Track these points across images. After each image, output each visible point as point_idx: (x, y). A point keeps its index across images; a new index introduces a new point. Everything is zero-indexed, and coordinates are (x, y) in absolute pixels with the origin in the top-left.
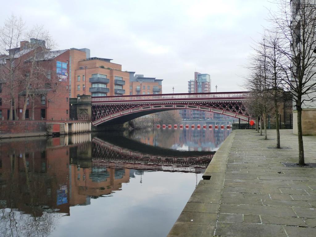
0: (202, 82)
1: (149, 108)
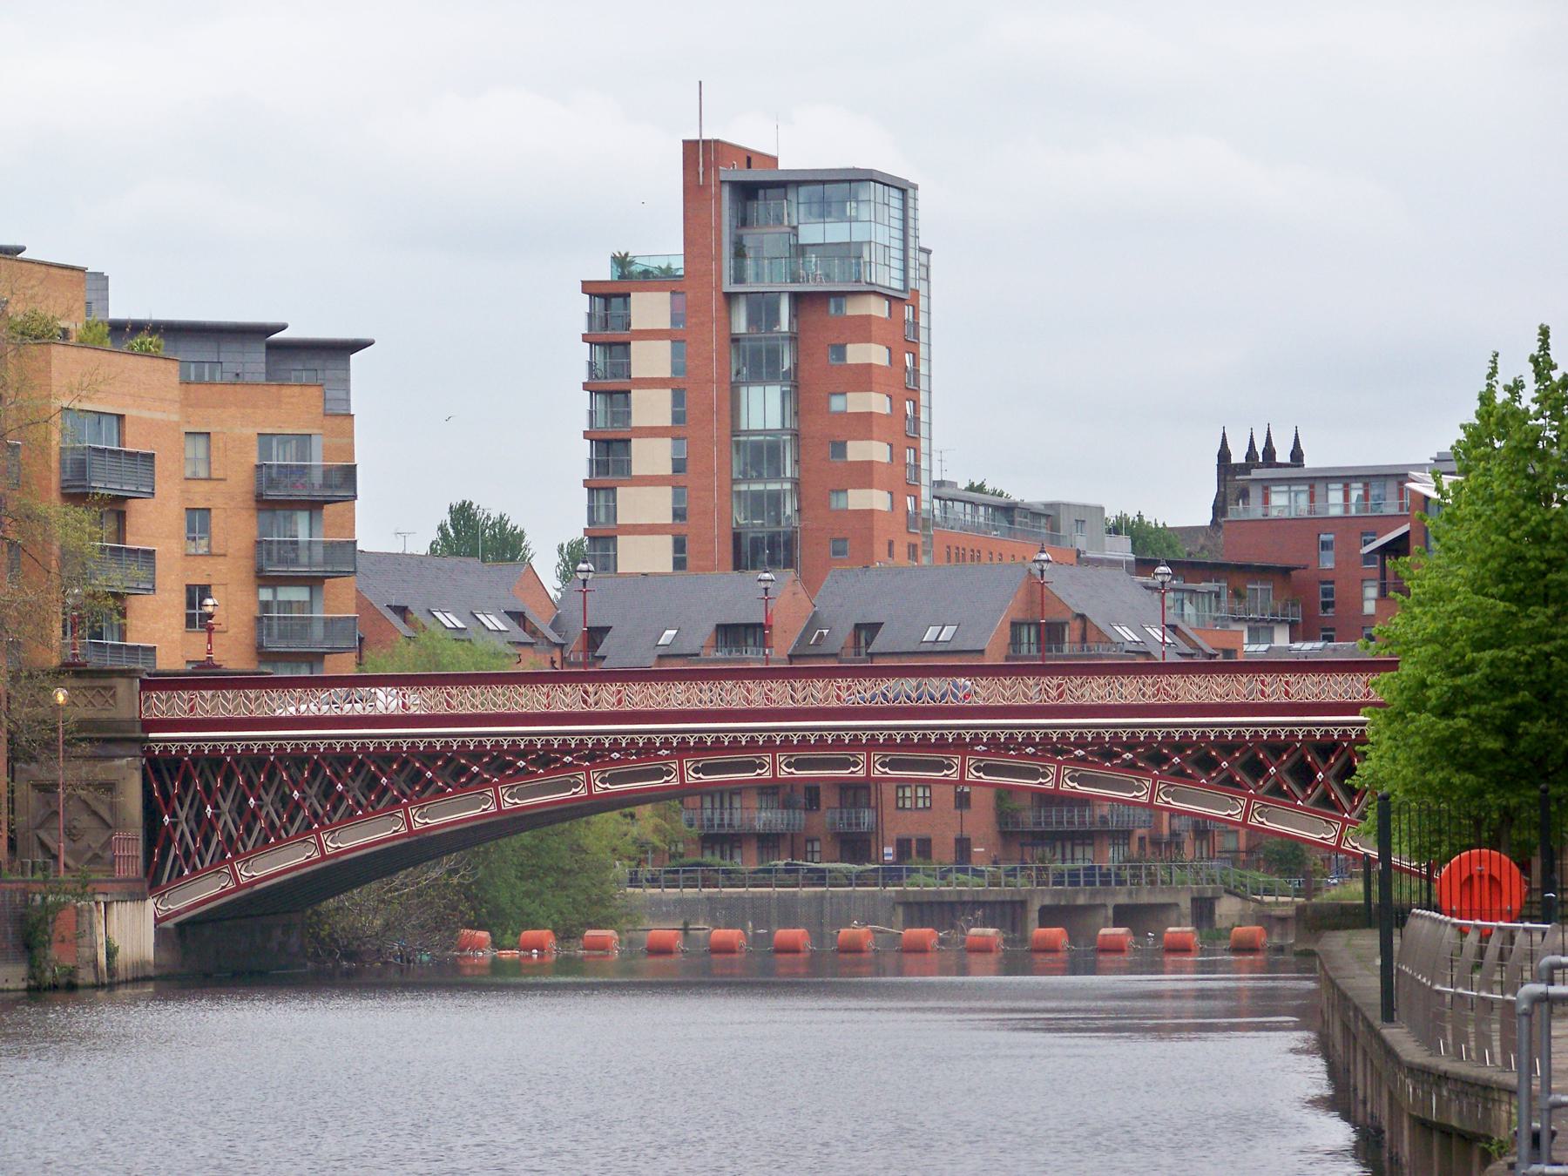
1: (658, 774)
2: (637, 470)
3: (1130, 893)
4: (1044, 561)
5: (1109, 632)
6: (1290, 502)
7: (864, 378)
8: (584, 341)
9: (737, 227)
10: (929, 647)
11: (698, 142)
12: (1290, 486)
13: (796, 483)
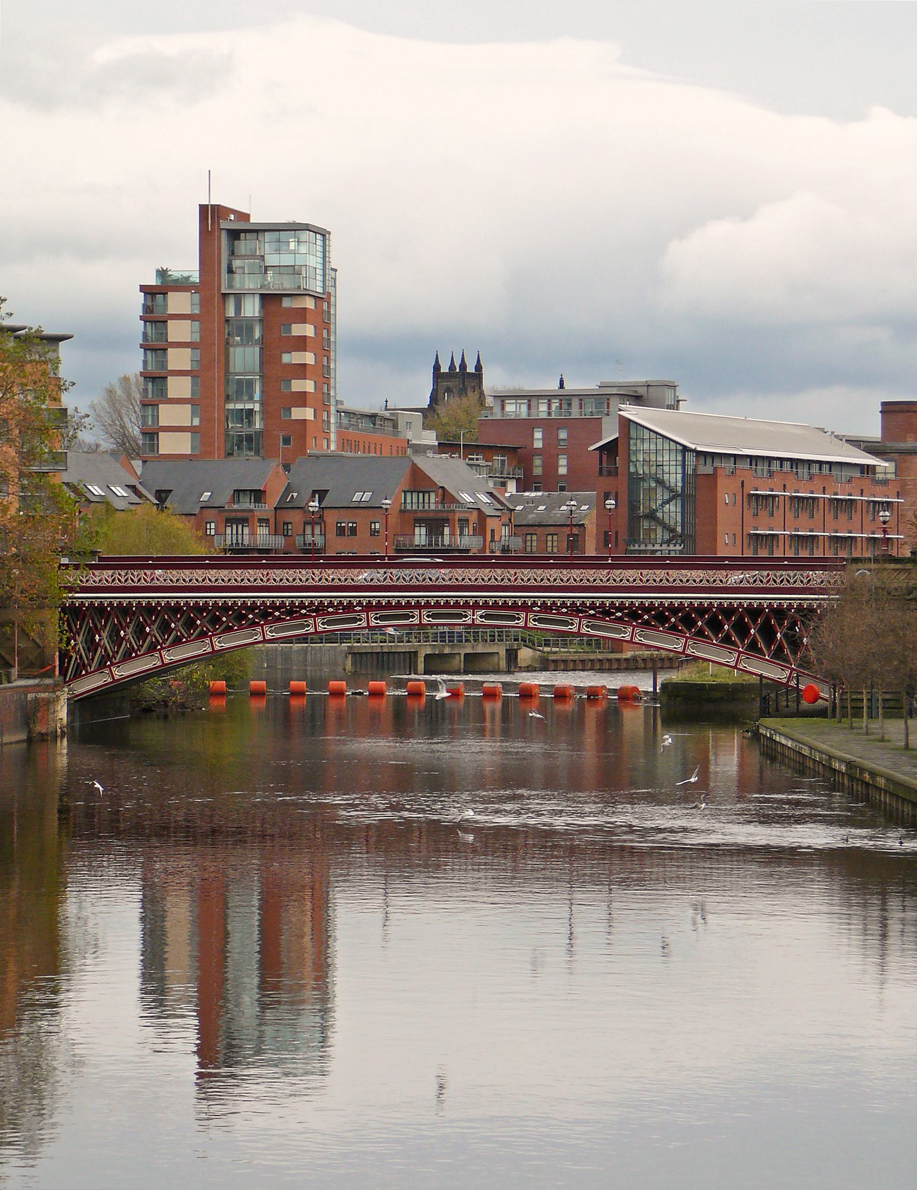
0: (269, 299)
1: (355, 620)
2: (171, 395)
3: (473, 647)
4: (573, 505)
5: (458, 497)
6: (516, 409)
7: (301, 343)
8: (140, 320)
9: (229, 255)
10: (356, 505)
11: (208, 205)
12: (516, 400)
13: (262, 403)
